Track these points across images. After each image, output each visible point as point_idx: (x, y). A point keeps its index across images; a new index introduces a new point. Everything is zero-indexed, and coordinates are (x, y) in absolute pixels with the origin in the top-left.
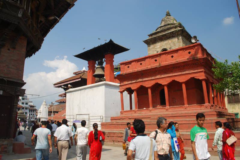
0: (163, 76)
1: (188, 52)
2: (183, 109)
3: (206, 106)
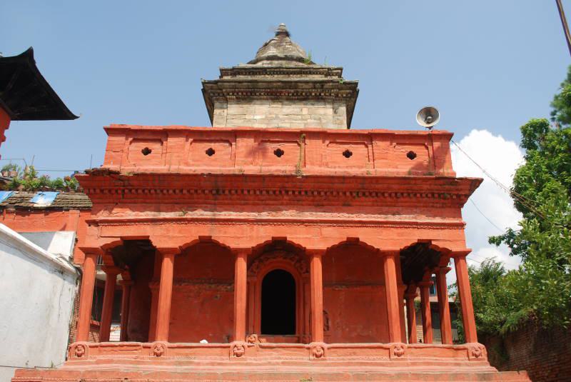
0: (308, 216)
1: (409, 150)
2: (306, 359)
3: (319, 353)
